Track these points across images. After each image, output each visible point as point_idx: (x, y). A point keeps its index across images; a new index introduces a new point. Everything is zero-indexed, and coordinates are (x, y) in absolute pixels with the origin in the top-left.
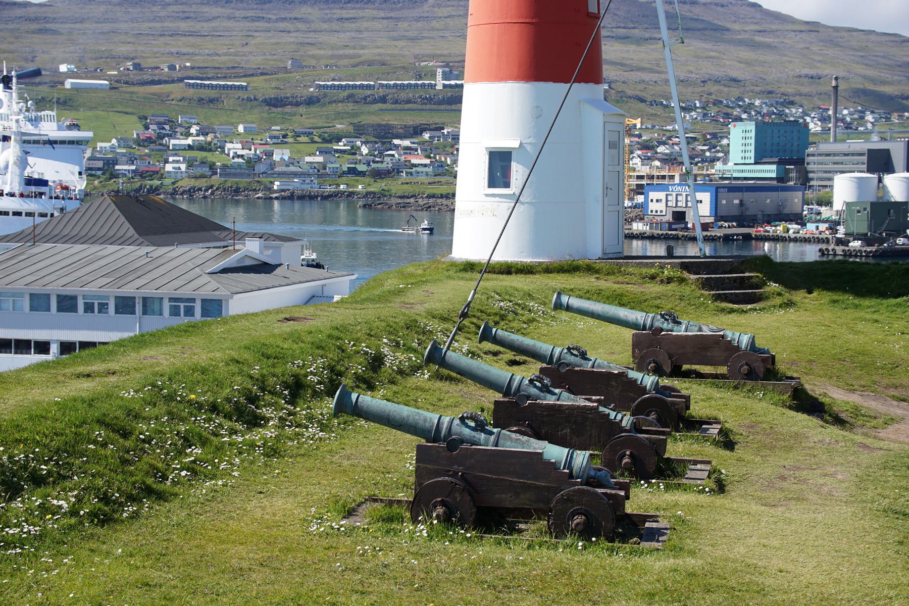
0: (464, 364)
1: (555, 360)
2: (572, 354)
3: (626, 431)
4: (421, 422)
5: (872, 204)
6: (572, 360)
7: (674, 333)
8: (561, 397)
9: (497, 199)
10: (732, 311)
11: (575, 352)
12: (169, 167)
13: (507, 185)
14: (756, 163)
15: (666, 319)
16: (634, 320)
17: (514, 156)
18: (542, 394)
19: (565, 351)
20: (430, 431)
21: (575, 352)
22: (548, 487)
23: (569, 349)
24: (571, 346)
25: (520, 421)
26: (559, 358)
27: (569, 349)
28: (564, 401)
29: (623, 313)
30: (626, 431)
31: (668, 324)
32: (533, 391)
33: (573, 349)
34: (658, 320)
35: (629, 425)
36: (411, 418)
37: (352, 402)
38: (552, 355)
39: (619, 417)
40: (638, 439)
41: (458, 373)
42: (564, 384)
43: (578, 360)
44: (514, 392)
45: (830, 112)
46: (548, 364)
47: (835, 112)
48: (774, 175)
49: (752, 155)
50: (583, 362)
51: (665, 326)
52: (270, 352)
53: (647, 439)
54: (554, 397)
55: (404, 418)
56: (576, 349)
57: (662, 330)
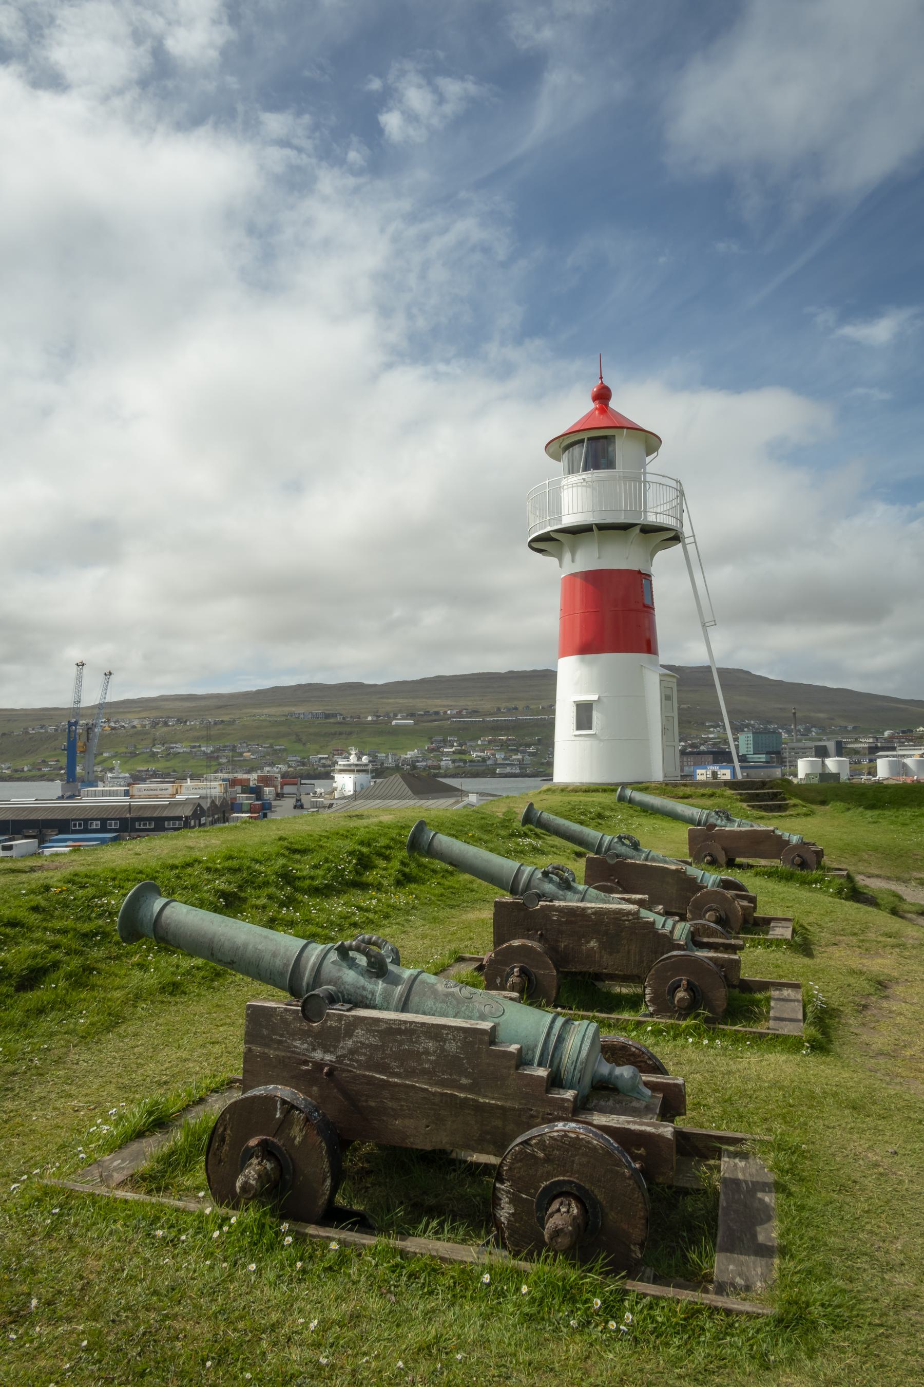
0: (458, 851)
1: (603, 849)
2: (623, 844)
3: (680, 947)
4: (268, 957)
5: (820, 774)
6: (623, 851)
7: (727, 829)
8: (587, 897)
9: (583, 738)
10: (761, 818)
11: (627, 842)
12: (443, 763)
13: (590, 728)
14: (754, 754)
15: (720, 816)
16: (691, 815)
17: (594, 706)
18: (561, 892)
19: (616, 840)
20: (282, 974)
21: (627, 842)
22: (502, 1108)
23: (620, 838)
24: (622, 835)
25: (529, 930)
26: (609, 848)
27: (620, 838)
28: (591, 902)
29: (681, 808)
30: (680, 947)
31: (722, 820)
32: (549, 887)
33: (625, 838)
34: (713, 817)
35: (684, 936)
36: (250, 947)
37: (152, 914)
38: (600, 845)
39: (669, 927)
40: (697, 960)
41: (451, 864)
42: (613, 878)
43: (631, 852)
44: (522, 890)
45: (792, 727)
46: (596, 854)
47: (795, 727)
48: (764, 760)
49: (752, 749)
50: (635, 853)
51: (719, 822)
52: (296, 847)
53: (710, 959)
54: (577, 896)
55: (238, 948)
56: (628, 839)
57: (716, 826)
